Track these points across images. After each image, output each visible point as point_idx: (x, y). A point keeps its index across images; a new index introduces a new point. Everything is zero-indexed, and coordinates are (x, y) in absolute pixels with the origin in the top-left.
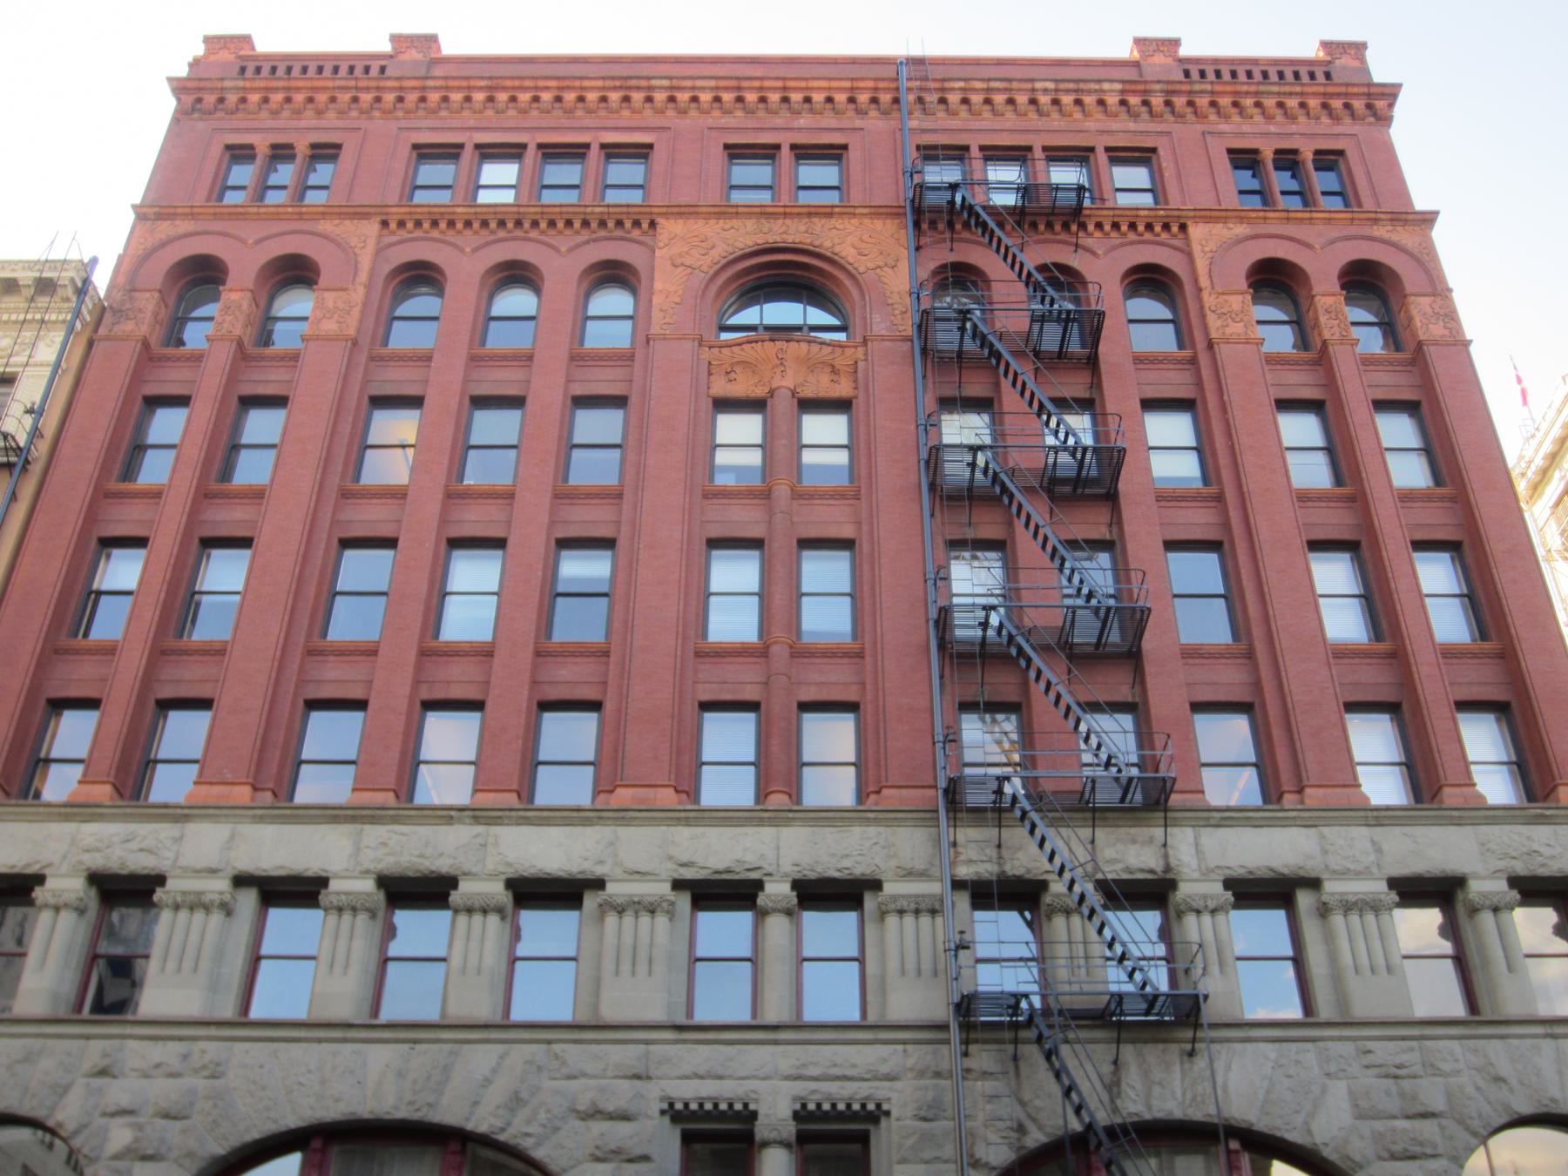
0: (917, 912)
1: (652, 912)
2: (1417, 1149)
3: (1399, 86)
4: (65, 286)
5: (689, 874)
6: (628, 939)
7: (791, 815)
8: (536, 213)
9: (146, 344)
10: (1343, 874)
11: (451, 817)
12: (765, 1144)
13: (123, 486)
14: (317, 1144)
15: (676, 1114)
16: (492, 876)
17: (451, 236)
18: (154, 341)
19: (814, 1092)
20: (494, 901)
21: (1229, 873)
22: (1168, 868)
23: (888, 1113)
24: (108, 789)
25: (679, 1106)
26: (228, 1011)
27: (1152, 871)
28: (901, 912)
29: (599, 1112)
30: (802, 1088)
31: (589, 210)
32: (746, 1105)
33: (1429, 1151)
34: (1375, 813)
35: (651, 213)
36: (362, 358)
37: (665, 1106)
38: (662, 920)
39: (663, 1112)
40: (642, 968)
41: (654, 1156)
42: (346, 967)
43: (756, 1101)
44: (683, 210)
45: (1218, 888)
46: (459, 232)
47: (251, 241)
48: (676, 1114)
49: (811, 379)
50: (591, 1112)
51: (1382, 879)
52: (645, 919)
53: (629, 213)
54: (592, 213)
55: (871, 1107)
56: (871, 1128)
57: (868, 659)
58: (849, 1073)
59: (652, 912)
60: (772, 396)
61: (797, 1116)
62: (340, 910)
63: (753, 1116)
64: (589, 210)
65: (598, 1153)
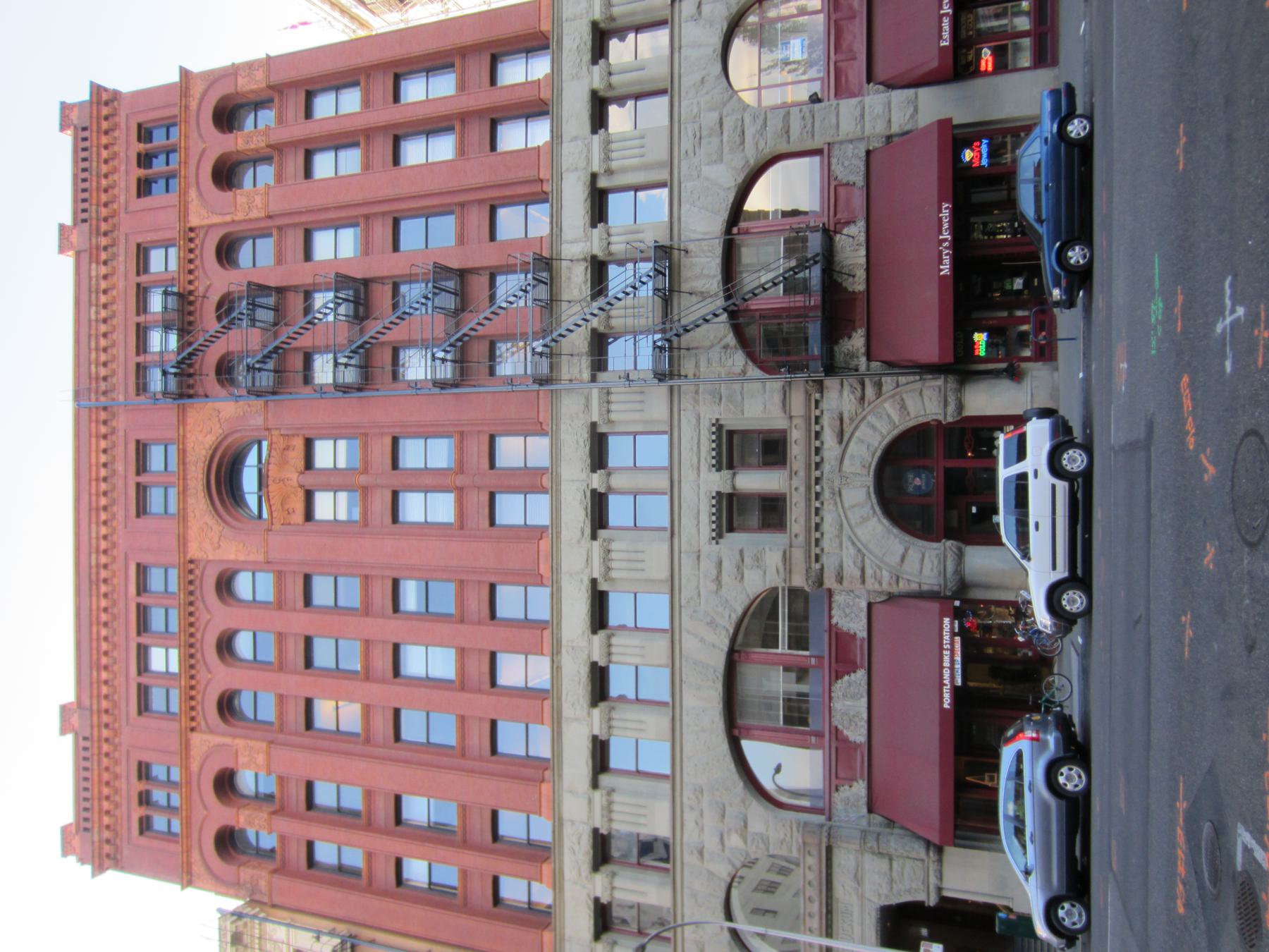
0: (608, 402)
5: (588, 531)
6: (624, 565)
9: (275, 871)
10: (589, 160)
12: (734, 487)
13: (277, 800)
14: (736, 732)
15: (718, 536)
16: (590, 642)
17: (200, 688)
18: (272, 866)
22: (585, 259)
23: (717, 420)
26: (667, 786)
28: (609, 411)
30: (704, 467)
33: (740, 123)
36: (282, 737)
42: (640, 722)
43: (711, 492)
45: (596, 231)
46: (198, 682)
47: (205, 812)
48: (718, 536)
59: (609, 551)
61: (719, 470)
63: (719, 493)
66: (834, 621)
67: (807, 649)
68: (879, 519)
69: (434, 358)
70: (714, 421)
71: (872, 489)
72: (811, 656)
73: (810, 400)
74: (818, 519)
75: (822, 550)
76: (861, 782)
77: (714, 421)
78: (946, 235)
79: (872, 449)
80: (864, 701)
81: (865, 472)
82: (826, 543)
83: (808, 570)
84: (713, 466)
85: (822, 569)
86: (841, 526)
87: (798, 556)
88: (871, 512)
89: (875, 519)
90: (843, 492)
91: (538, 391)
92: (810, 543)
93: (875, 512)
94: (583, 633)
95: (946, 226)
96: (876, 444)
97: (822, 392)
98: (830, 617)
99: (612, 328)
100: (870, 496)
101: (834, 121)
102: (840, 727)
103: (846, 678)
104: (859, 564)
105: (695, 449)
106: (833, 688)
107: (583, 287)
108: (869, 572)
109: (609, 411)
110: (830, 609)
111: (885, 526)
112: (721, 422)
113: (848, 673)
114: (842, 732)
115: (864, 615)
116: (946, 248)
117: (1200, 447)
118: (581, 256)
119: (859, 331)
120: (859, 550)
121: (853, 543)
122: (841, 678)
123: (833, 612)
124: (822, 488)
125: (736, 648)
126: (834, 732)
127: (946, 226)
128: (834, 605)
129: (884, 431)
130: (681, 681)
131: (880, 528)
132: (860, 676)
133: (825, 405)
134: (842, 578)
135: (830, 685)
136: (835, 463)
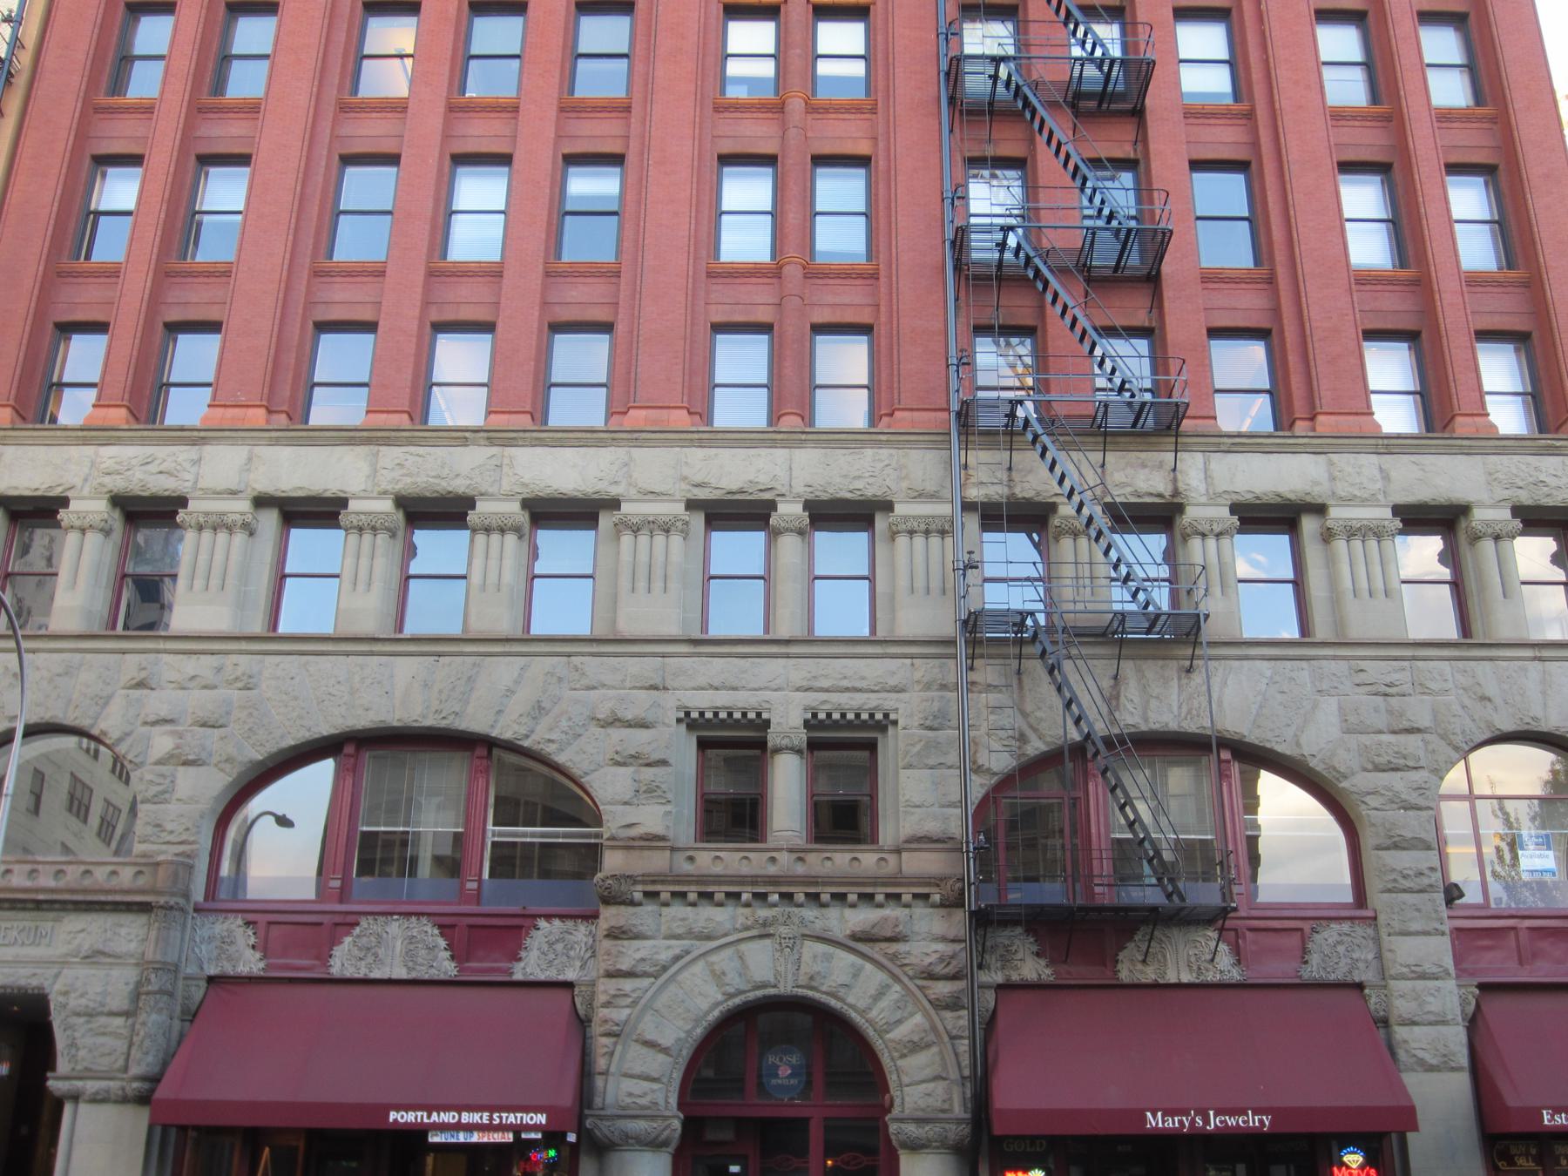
0: (927, 533)
1: (667, 531)
2: (1402, 762)
5: (702, 494)
6: (643, 557)
7: (803, 437)
10: (1349, 501)
16: (509, 496)
19: (825, 702)
21: (1236, 498)
22: (1176, 493)
24: (123, 412)
26: (257, 626)
27: (1160, 495)
29: (619, 720)
30: (813, 699)
32: (759, 715)
33: (1411, 764)
34: (1386, 442)
37: (682, 715)
38: (676, 540)
39: (679, 721)
40: (658, 585)
48: (691, 722)
50: (610, 720)
51: (1388, 506)
52: (660, 539)
55: (879, 716)
57: (883, 280)
58: (858, 684)
62: (361, 529)
63: (767, 723)
65: (616, 757)
66: (542, 923)
67: (491, 875)
68: (717, 1004)
70: (892, 717)
71: (772, 991)
72: (480, 881)
76: (261, 965)
77: (892, 717)
78: (1214, 1122)
79: (842, 994)
80: (400, 973)
81: (803, 980)
82: (678, 910)
84: (815, 715)
86: (709, 938)
87: (657, 862)
89: (720, 997)
90: (767, 942)
91: (948, 410)
92: (679, 882)
93: (731, 996)
95: (1231, 1121)
96: (851, 1000)
97: (942, 905)
98: (548, 917)
99: (1057, 540)
101: (1414, 927)
102: (357, 930)
103: (442, 943)
105: (845, 683)
106: (424, 920)
107: (1129, 489)
109: (911, 533)
110: (562, 917)
111: (707, 1013)
113: (450, 947)
114: (348, 934)
115: (550, 974)
116: (1193, 1122)
118: (1181, 486)
119: (1048, 971)
120: (665, 969)
121: (677, 958)
122: (442, 935)
123: (557, 922)
124: (775, 905)
125: (496, 751)
126: (350, 919)
127: (1231, 1121)
128: (570, 924)
129: (873, 1014)
130: (439, 655)
131: (704, 1005)
132: (446, 967)
133: (920, 910)
135: (429, 914)
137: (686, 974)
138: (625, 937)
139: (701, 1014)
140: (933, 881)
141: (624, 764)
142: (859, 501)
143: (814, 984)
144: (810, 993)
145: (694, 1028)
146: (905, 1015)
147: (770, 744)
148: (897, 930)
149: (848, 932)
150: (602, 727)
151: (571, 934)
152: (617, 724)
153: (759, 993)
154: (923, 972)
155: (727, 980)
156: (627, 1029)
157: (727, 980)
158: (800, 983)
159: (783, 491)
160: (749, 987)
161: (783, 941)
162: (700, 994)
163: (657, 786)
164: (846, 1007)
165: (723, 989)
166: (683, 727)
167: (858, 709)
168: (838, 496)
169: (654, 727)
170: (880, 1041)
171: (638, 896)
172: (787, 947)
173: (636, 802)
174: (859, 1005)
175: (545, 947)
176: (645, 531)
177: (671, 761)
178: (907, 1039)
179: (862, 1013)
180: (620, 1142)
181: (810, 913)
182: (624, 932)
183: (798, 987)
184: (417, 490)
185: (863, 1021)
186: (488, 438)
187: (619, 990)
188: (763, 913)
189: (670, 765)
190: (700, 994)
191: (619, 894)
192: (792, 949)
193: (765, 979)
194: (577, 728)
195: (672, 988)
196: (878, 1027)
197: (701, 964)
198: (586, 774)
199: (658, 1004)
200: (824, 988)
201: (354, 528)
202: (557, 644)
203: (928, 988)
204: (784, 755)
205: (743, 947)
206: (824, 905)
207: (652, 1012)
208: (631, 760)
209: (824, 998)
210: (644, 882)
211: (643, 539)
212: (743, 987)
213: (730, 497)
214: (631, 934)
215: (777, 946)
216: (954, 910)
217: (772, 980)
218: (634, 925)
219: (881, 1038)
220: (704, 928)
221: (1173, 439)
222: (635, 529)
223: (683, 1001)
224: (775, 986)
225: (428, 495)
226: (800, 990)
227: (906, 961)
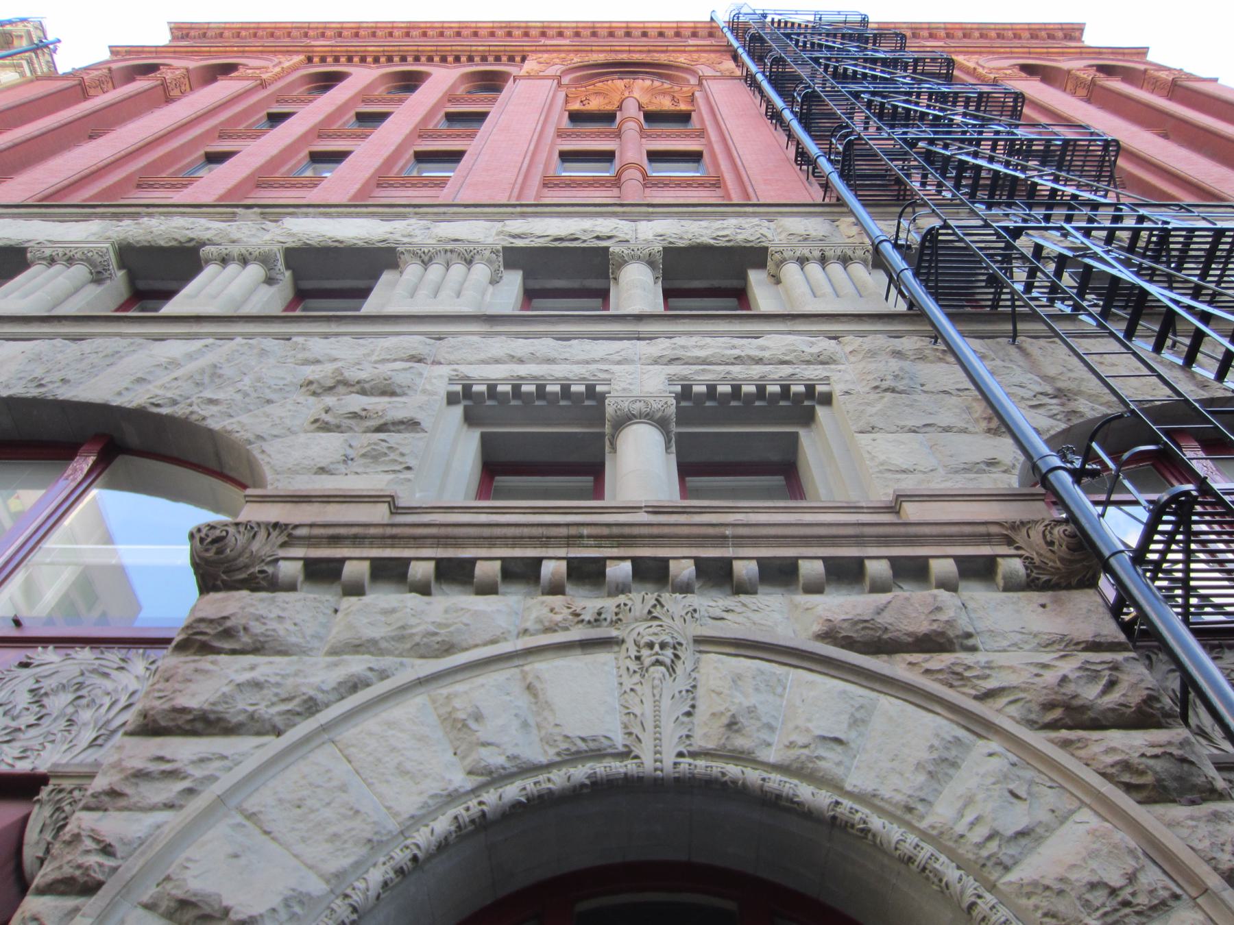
0: (823, 260)
1: (469, 262)
3: (1084, 24)
4: (21, 37)
7: (651, 210)
8: (432, 51)
11: (234, 214)
12: (624, 420)
20: (483, 764)
23: (827, 399)
25: (480, 388)
28: (802, 261)
29: (345, 383)
31: (474, 48)
35: (523, 51)
41: (426, 424)
42: (26, 296)
44: (549, 48)
49: (654, 101)
50: (330, 383)
52: (458, 269)
53: (505, 51)
54: (476, 51)
56: (802, 433)
59: (469, 262)
60: (621, 110)
61: (680, 397)
63: (602, 398)
64: (474, 48)
65: (327, 418)
68: (453, 797)
69: (662, 771)
71: (618, 767)
73: (987, 539)
74: (487, 570)
75: (355, 590)
79: (830, 760)
81: (706, 734)
82: (384, 598)
83: (287, 534)
85: (273, 585)
88: (495, 759)
89: (459, 780)
90: (604, 658)
93: (496, 778)
94: (293, 235)
96: (854, 781)
97: (1031, 584)
100: (576, 757)
104: (243, 704)
108: (183, 750)
109: (802, 261)
111: (416, 821)
112: (821, 411)
117: (234, 512)
120: (311, 706)
121: (354, 685)
124: (621, 589)
129: (942, 813)
131: (408, 801)
133: (977, 595)
134: (206, 649)
136: (734, 627)
137: (371, 723)
138: (227, 645)
139: (393, 825)
140: (994, 529)
141: (338, 428)
142: (726, 248)
143: (740, 742)
144: (733, 770)
145: (359, 866)
146: (1043, 815)
147: (610, 410)
148: (943, 617)
149: (816, 628)
150: (314, 394)
151: (106, 675)
152: (341, 389)
153: (580, 772)
154: (1048, 706)
155: (483, 732)
156: (131, 867)
157: (483, 732)
158: (699, 742)
159: (627, 237)
160: (550, 755)
161: (645, 652)
162: (402, 771)
163: (390, 448)
164: (847, 803)
165: (469, 762)
166: (458, 411)
167: (762, 378)
168: (698, 241)
169: (404, 394)
170: (990, 898)
171: (290, 569)
172: (658, 663)
173: (344, 471)
174: (886, 792)
175: (23, 699)
176: (440, 259)
177: (424, 425)
178: (1084, 876)
179: (906, 812)
180: (1016, 818)
181: (709, 602)
182: (228, 633)
183: (694, 755)
184: (149, 238)
185: (912, 839)
186: (262, 213)
187: (161, 759)
188: (589, 602)
189: (424, 431)
190: (402, 771)
191: (243, 560)
192: (672, 669)
193: (598, 731)
194: (267, 391)
195: (324, 757)
196: (965, 851)
197: (417, 702)
198: (260, 437)
199: (261, 799)
200: (772, 756)
201: (44, 259)
202: (272, 322)
203: (1085, 744)
204: (635, 427)
205: (542, 667)
206: (741, 589)
207: (239, 819)
208: (352, 422)
209: (776, 782)
210: (310, 541)
211: (435, 270)
212: (536, 753)
213: (557, 244)
214: (246, 639)
215: (634, 666)
216: (1063, 594)
217: (620, 740)
218: (260, 618)
219: (992, 888)
220: (440, 625)
221: (1010, 327)
222: (426, 258)
223: (343, 788)
224: (626, 754)
225: (162, 243)
226: (701, 763)
227: (991, 684)
